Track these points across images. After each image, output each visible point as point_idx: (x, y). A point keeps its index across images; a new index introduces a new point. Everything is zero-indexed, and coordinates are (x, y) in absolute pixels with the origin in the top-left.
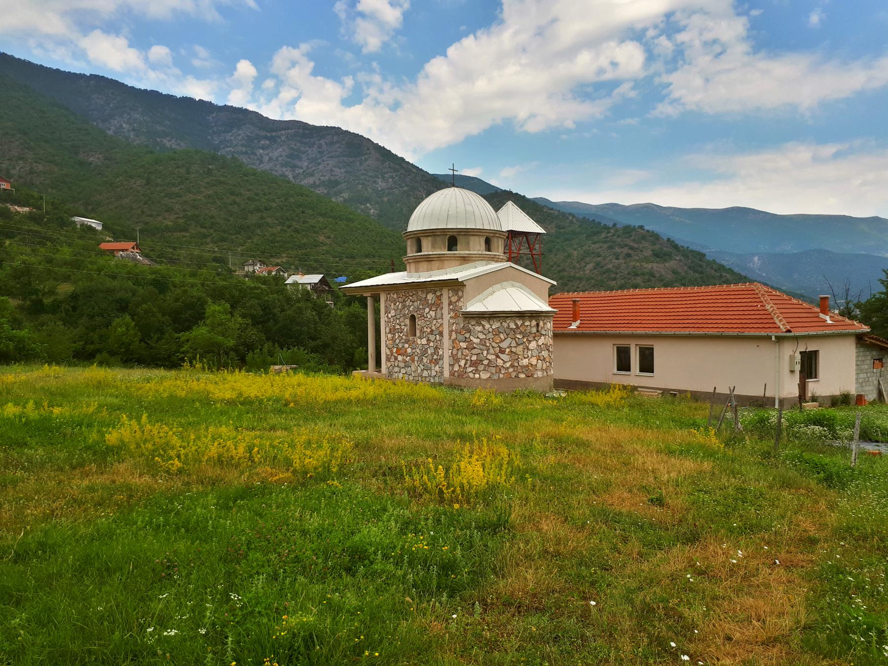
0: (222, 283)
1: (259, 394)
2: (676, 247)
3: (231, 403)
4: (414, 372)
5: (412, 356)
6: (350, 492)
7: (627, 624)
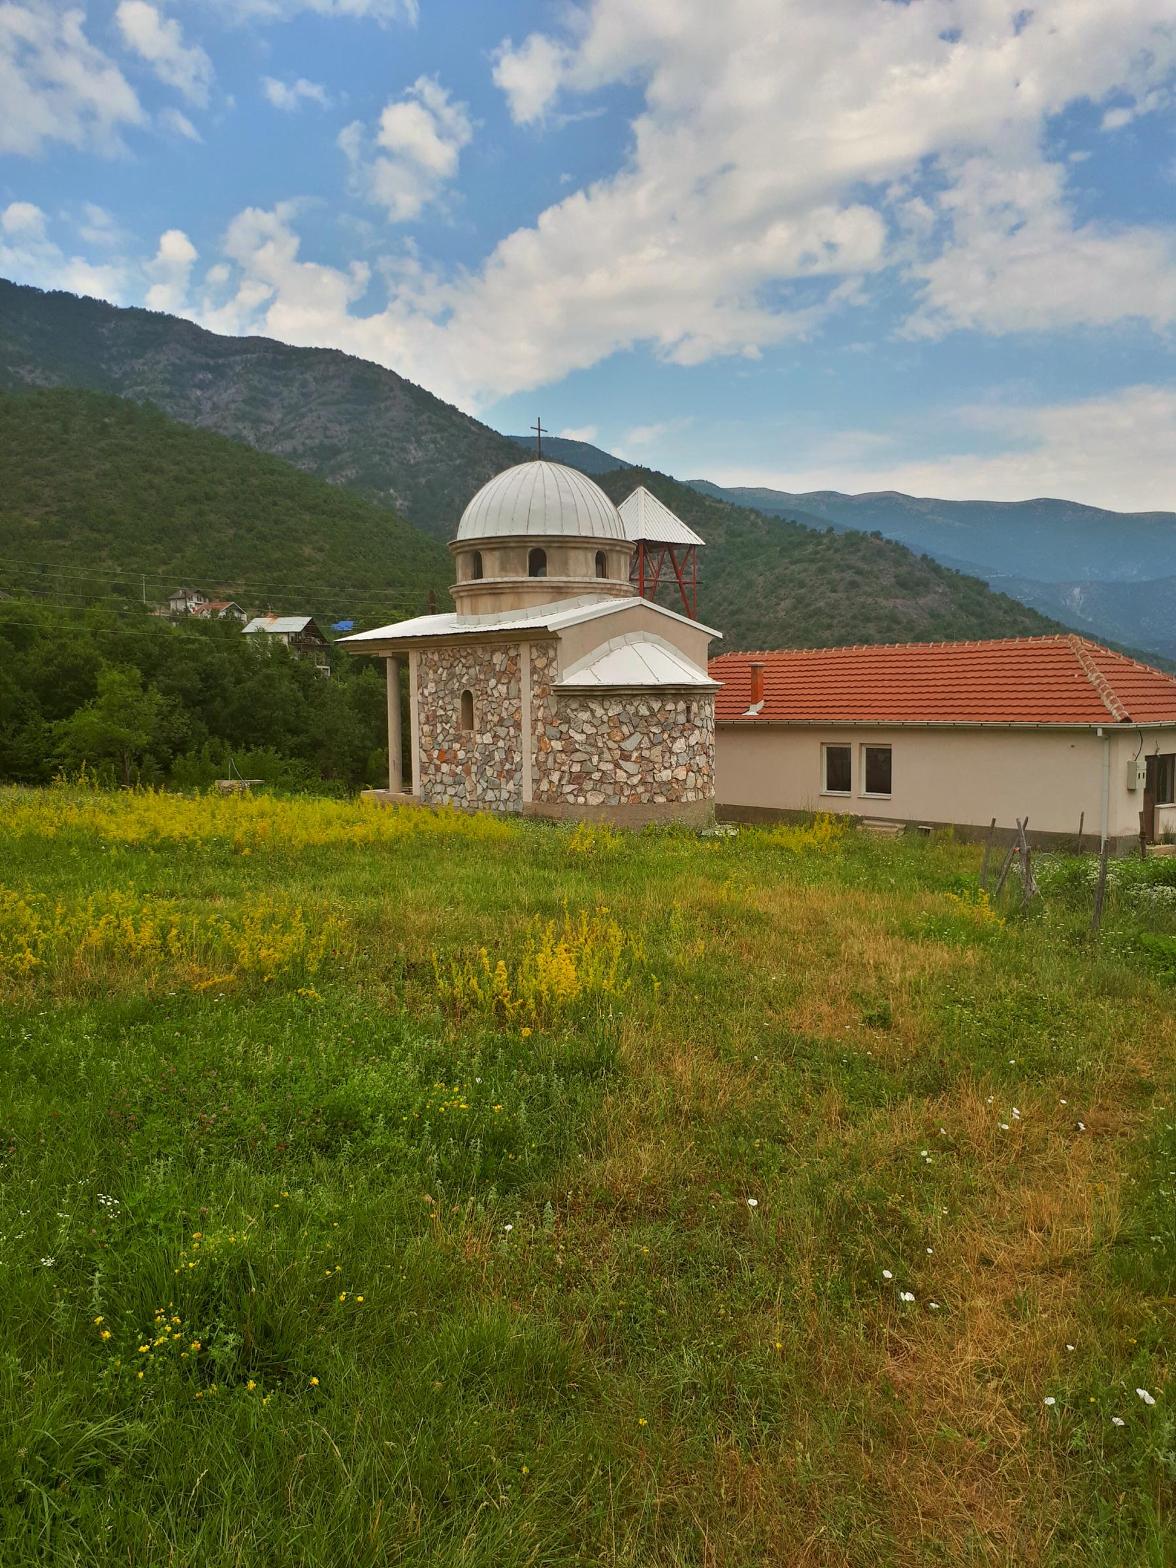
0: (129, 632)
1: (187, 833)
2: (936, 569)
3: (137, 848)
4: (471, 792)
5: (465, 764)
6: (339, 1009)
7: (810, 1240)
